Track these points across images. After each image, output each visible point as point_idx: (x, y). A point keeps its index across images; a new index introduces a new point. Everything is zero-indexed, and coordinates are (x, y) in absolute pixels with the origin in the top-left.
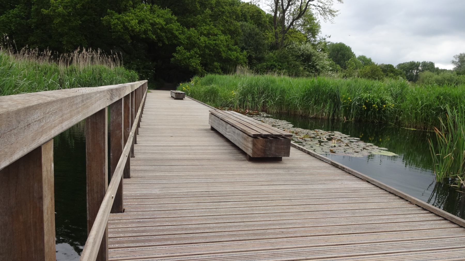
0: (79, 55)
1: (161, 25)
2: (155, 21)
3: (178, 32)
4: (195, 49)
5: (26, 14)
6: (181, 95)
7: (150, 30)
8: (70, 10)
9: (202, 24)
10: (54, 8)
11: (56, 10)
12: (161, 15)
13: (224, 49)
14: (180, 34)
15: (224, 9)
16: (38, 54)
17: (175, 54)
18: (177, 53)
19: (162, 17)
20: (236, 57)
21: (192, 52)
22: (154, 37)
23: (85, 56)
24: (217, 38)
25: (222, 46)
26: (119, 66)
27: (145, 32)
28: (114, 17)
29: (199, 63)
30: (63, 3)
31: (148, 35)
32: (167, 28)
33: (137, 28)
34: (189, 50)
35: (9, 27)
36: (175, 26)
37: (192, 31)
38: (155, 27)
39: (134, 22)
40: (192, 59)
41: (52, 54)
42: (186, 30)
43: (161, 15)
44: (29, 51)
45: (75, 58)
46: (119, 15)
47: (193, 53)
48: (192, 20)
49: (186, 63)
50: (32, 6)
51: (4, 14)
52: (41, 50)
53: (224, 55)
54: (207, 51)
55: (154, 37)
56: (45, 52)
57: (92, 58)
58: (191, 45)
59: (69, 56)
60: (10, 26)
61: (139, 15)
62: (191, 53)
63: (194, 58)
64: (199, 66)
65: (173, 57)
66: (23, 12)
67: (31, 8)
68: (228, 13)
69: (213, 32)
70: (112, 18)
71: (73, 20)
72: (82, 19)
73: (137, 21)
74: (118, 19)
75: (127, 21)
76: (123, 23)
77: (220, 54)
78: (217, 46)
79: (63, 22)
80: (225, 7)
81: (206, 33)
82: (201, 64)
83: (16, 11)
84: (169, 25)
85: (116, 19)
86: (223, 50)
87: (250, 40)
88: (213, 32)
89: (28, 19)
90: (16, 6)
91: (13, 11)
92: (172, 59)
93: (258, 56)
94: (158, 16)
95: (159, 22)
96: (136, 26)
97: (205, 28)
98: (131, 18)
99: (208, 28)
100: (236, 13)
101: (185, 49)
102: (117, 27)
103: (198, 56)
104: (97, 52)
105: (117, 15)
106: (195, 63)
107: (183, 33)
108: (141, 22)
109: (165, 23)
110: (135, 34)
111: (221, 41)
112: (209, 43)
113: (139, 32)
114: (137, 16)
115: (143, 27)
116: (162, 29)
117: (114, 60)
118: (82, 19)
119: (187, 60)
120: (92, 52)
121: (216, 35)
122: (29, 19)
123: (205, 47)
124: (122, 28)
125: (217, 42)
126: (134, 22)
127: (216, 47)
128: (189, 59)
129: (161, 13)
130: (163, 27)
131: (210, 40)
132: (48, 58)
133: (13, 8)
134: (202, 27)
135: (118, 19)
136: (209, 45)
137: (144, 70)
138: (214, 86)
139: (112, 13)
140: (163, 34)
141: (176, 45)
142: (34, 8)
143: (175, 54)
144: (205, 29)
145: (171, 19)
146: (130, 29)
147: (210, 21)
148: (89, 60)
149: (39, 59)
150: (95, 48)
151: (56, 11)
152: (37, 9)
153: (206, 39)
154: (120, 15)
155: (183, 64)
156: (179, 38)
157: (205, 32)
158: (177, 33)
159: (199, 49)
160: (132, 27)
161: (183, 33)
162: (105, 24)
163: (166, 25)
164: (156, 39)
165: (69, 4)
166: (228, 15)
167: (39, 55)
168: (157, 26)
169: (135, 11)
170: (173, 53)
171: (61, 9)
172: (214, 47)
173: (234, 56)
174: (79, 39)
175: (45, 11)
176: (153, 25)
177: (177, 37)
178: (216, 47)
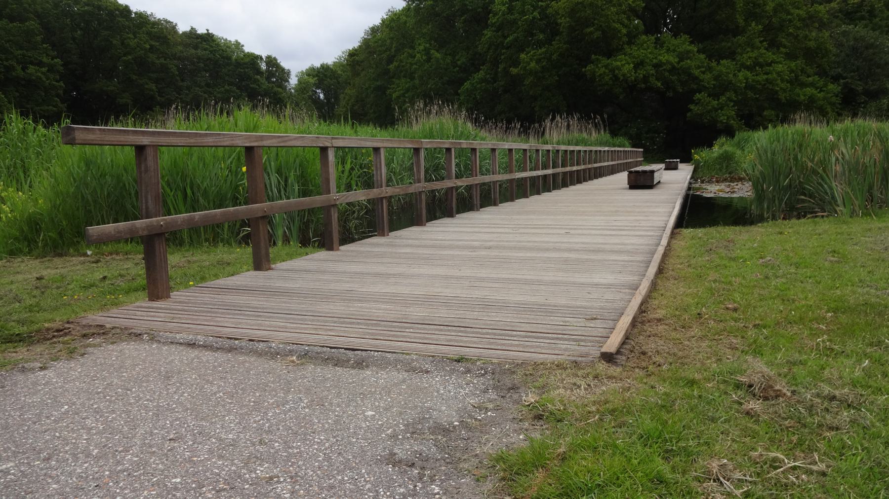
0: (552, 124)
1: (671, 64)
2: (660, 61)
3: (699, 71)
4: (728, 94)
5: (492, 76)
6: (673, 163)
7: (653, 75)
8: (544, 63)
9: (746, 49)
10: (525, 65)
11: (526, 67)
12: (672, 48)
13: (783, 85)
14: (703, 73)
15: (792, 14)
16: (506, 127)
17: (692, 107)
18: (697, 104)
19: (674, 51)
20: (809, 98)
21: (723, 99)
22: (659, 84)
23: (560, 125)
24: (772, 69)
25: (779, 81)
26: (603, 133)
27: (646, 78)
28: (599, 65)
29: (735, 116)
30: (535, 56)
31: (650, 82)
32: (681, 67)
33: (632, 75)
34: (715, 96)
35: (474, 96)
36: (696, 62)
37: (725, 66)
38: (661, 69)
39: (628, 68)
40: (721, 111)
41: (521, 126)
42: (714, 64)
43: (672, 48)
44: (497, 126)
45: (548, 128)
46: (608, 59)
47: (724, 100)
48: (729, 44)
49: (712, 117)
50: (500, 66)
51: (469, 79)
52: (509, 122)
53: (782, 96)
54: (750, 94)
55: (659, 84)
56: (513, 125)
57: (568, 126)
58: (721, 87)
59: (540, 126)
60: (475, 95)
61: (636, 56)
62: (721, 101)
63: (725, 108)
64: (734, 120)
65: (690, 110)
66: (489, 73)
67: (498, 68)
68: (799, 20)
69: (764, 60)
70: (597, 67)
71: (547, 76)
72: (560, 73)
73: (632, 65)
74: (606, 67)
75: (619, 68)
76: (612, 71)
77: (775, 96)
78: (770, 83)
79: (535, 81)
80: (792, 11)
81: (750, 64)
82: (738, 115)
83: (481, 74)
84: (684, 63)
85: (602, 67)
86: (781, 88)
87: (852, 61)
88: (764, 60)
89: (495, 82)
90: (481, 67)
91: (478, 75)
92: (689, 114)
93: (871, 88)
94: (668, 50)
95: (667, 60)
96: (630, 74)
97: (748, 56)
98: (623, 62)
99: (754, 55)
100: (816, 17)
101: (709, 96)
102: (603, 78)
103: (732, 104)
104: (574, 118)
105: (605, 61)
106: (727, 115)
107: (710, 69)
108: (639, 65)
109: (677, 60)
110: (630, 84)
111: (778, 73)
112: (753, 81)
113: (635, 80)
114: (634, 57)
115: (641, 73)
116: (673, 70)
117: (596, 126)
118: (560, 73)
119: (714, 112)
120: (567, 118)
121: (177, 238)
122: (495, 82)
123: (746, 87)
124: (611, 79)
125: (770, 76)
126: (628, 68)
127: (768, 85)
128: (716, 110)
129: (673, 45)
130: (674, 67)
131: (757, 75)
132: (517, 132)
133: (478, 70)
134: (744, 55)
135: (606, 67)
136: (755, 83)
137: (648, 136)
138: (727, 149)
139: (598, 59)
140: (674, 78)
141: (694, 92)
142: (501, 67)
143: (692, 107)
144: (750, 58)
145: (689, 52)
146: (622, 78)
147: (761, 42)
148: (564, 130)
149: (507, 133)
150: (570, 113)
151: (528, 68)
152: (505, 68)
153: (749, 74)
154: (609, 61)
155: (706, 121)
156: (701, 81)
157: (749, 63)
158: (696, 72)
159: (736, 92)
160: (624, 75)
161: (710, 69)
162: (588, 76)
163: (678, 63)
164: (662, 87)
165: (543, 56)
166: (798, 24)
167: (507, 128)
168: (665, 67)
169: (631, 49)
170: (690, 105)
171: (533, 64)
172: (765, 85)
173: (805, 95)
174: (555, 101)
175: (514, 71)
176: (656, 66)
177: (697, 78)
178: (768, 85)
